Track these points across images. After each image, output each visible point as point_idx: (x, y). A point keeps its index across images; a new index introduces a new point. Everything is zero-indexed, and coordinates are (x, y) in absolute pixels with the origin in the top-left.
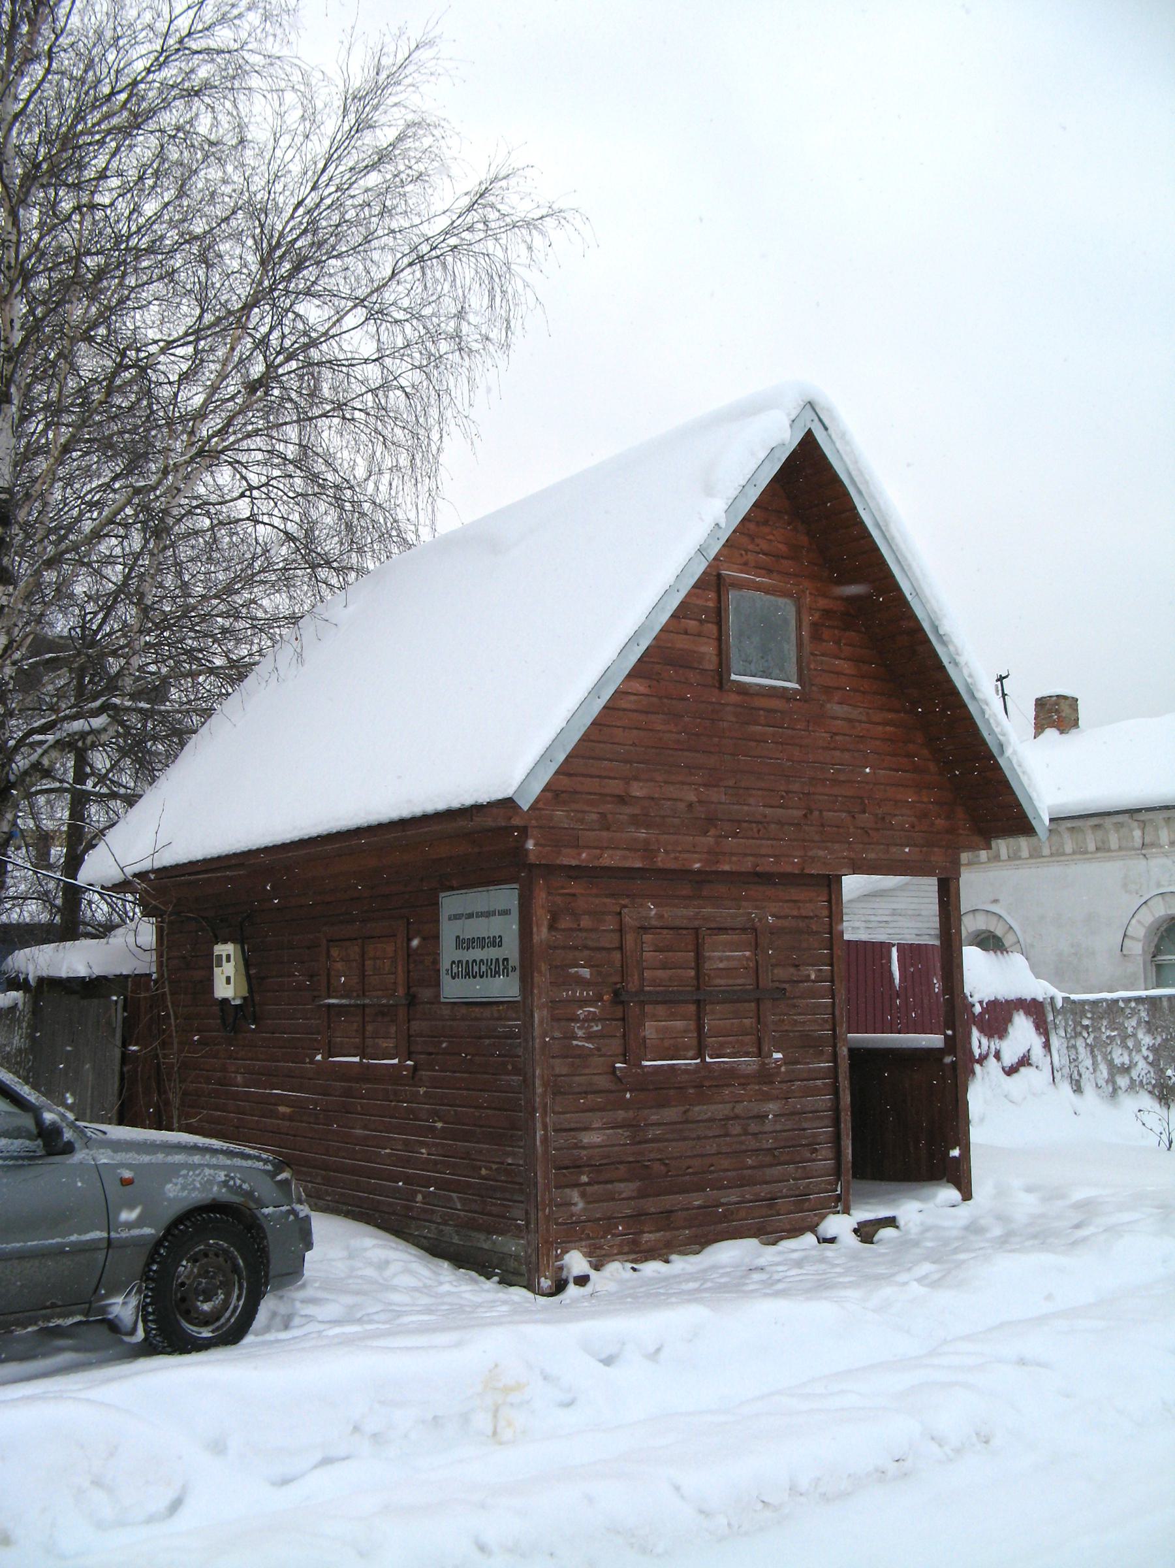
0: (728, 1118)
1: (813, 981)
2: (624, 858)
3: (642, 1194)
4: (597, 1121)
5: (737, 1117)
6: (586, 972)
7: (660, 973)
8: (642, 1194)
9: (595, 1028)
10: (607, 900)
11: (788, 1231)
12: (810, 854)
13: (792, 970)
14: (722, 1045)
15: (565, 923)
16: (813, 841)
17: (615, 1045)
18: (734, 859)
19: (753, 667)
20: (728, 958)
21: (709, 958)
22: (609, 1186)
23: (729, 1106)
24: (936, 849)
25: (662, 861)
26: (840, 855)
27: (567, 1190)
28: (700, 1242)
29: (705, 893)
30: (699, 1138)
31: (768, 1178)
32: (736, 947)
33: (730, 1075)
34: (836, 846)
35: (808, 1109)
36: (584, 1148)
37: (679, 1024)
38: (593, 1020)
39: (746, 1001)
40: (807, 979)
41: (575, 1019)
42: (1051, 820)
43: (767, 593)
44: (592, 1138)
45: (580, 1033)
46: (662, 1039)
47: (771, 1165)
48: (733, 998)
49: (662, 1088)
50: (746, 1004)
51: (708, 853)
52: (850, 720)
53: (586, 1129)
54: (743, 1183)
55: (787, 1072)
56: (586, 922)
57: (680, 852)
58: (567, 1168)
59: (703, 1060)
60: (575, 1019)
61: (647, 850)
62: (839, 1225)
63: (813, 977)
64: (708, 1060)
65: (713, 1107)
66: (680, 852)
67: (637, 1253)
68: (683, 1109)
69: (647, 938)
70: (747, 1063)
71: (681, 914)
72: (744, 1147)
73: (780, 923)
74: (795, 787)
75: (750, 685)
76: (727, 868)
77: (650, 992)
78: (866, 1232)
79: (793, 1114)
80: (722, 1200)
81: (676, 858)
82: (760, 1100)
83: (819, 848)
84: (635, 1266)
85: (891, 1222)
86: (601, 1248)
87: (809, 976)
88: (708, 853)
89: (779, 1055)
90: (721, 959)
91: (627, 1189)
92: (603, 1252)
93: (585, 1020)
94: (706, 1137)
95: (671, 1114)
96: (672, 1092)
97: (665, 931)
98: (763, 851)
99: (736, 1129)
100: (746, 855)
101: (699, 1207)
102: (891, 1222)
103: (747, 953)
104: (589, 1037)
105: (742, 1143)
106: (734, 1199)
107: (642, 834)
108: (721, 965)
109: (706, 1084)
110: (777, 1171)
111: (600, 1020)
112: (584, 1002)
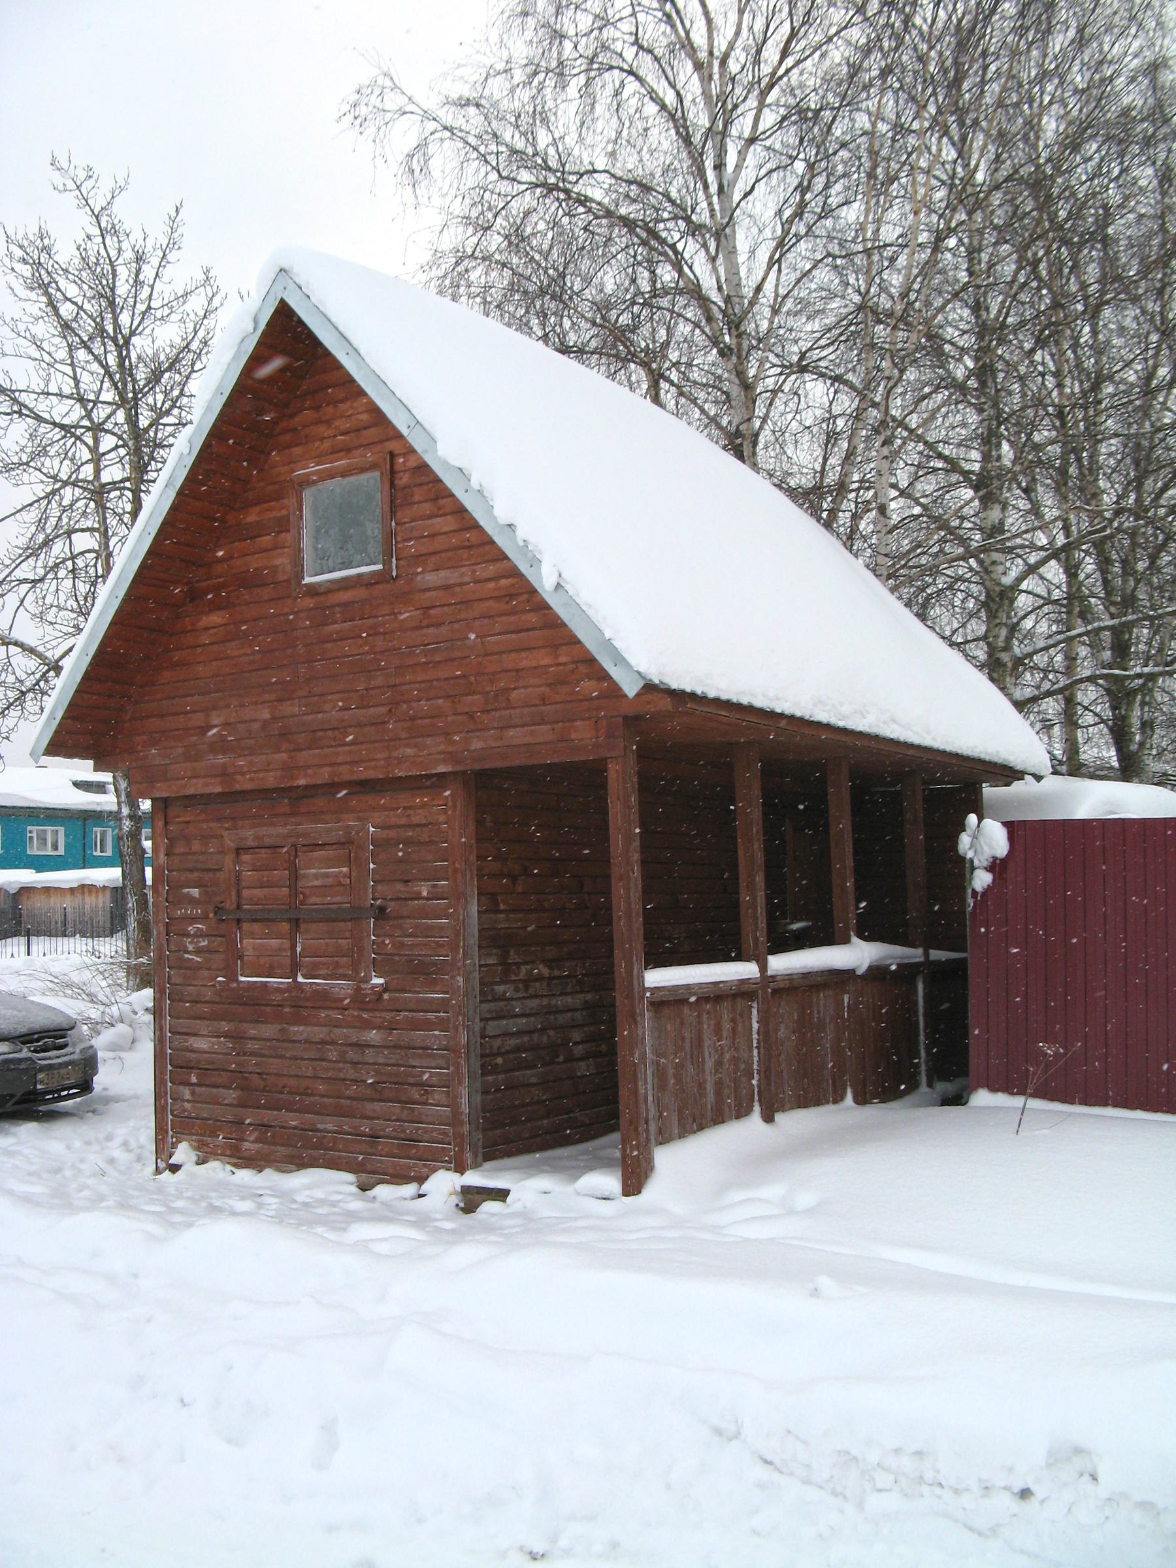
0: (323, 1042)
1: (427, 899)
2: (207, 785)
3: (242, 1104)
4: (204, 1027)
5: (333, 1043)
6: (195, 892)
7: (257, 891)
8: (242, 1104)
9: (203, 944)
10: (215, 824)
11: (392, 1176)
12: (395, 754)
13: (399, 886)
14: (316, 966)
15: (180, 849)
16: (400, 739)
17: (218, 960)
18: (310, 771)
19: (330, 562)
20: (327, 875)
21: (305, 876)
22: (215, 1090)
23: (325, 1029)
24: (578, 723)
25: (244, 783)
26: (433, 750)
27: (181, 1087)
28: (300, 1163)
29: (302, 810)
30: (295, 1058)
31: (368, 1113)
32: (330, 863)
33: (323, 999)
34: (429, 741)
35: (417, 1044)
36: (193, 1051)
37: (274, 943)
38: (201, 936)
39: (344, 921)
40: (418, 897)
41: (188, 935)
42: (83, 731)
43: (343, 476)
44: (202, 1044)
45: (191, 948)
46: (258, 957)
47: (373, 1100)
48: (330, 917)
49: (255, 1004)
50: (342, 924)
51: (283, 769)
52: (446, 588)
53: (195, 1035)
54: (339, 1112)
55: (390, 1000)
56: (196, 846)
57: (255, 772)
58: (181, 1067)
59: (295, 980)
60: (188, 935)
61: (224, 774)
62: (444, 1184)
63: (425, 894)
64: (300, 979)
65: (309, 1029)
66: (255, 772)
67: (239, 1158)
68: (279, 1027)
69: (246, 858)
70: (342, 986)
71: (274, 832)
72: (341, 1075)
73: (384, 834)
74: (379, 681)
75: (319, 584)
76: (302, 782)
77: (249, 911)
78: (471, 1199)
79: (396, 1047)
80: (319, 1126)
81: (251, 779)
82: (360, 1028)
83: (407, 746)
84: (234, 1170)
85: (501, 1195)
86: (207, 1145)
87: (420, 893)
88: (283, 769)
89: (381, 981)
90: (316, 877)
91: (232, 1095)
92: (209, 1150)
93: (195, 936)
94: (302, 1059)
95: (268, 1030)
96: (268, 1009)
97: (264, 850)
98: (340, 759)
99: (333, 1055)
100: (320, 766)
101: (295, 1128)
102: (501, 1195)
103: (345, 869)
104: (198, 952)
105: (340, 1070)
106: (330, 1127)
107: (221, 759)
108: (316, 883)
109: (303, 1005)
110: (378, 1107)
111: (207, 936)
112: (194, 919)
